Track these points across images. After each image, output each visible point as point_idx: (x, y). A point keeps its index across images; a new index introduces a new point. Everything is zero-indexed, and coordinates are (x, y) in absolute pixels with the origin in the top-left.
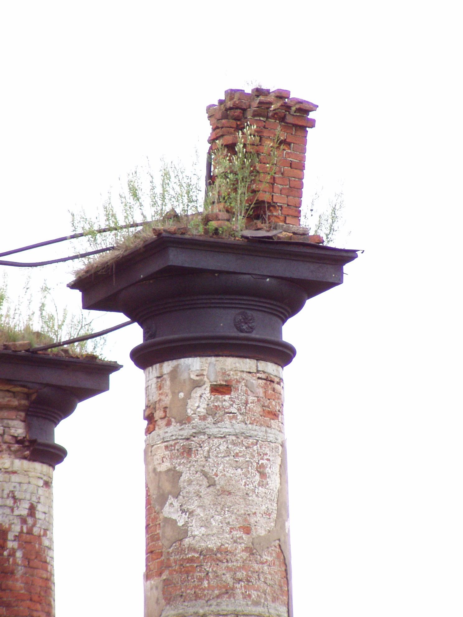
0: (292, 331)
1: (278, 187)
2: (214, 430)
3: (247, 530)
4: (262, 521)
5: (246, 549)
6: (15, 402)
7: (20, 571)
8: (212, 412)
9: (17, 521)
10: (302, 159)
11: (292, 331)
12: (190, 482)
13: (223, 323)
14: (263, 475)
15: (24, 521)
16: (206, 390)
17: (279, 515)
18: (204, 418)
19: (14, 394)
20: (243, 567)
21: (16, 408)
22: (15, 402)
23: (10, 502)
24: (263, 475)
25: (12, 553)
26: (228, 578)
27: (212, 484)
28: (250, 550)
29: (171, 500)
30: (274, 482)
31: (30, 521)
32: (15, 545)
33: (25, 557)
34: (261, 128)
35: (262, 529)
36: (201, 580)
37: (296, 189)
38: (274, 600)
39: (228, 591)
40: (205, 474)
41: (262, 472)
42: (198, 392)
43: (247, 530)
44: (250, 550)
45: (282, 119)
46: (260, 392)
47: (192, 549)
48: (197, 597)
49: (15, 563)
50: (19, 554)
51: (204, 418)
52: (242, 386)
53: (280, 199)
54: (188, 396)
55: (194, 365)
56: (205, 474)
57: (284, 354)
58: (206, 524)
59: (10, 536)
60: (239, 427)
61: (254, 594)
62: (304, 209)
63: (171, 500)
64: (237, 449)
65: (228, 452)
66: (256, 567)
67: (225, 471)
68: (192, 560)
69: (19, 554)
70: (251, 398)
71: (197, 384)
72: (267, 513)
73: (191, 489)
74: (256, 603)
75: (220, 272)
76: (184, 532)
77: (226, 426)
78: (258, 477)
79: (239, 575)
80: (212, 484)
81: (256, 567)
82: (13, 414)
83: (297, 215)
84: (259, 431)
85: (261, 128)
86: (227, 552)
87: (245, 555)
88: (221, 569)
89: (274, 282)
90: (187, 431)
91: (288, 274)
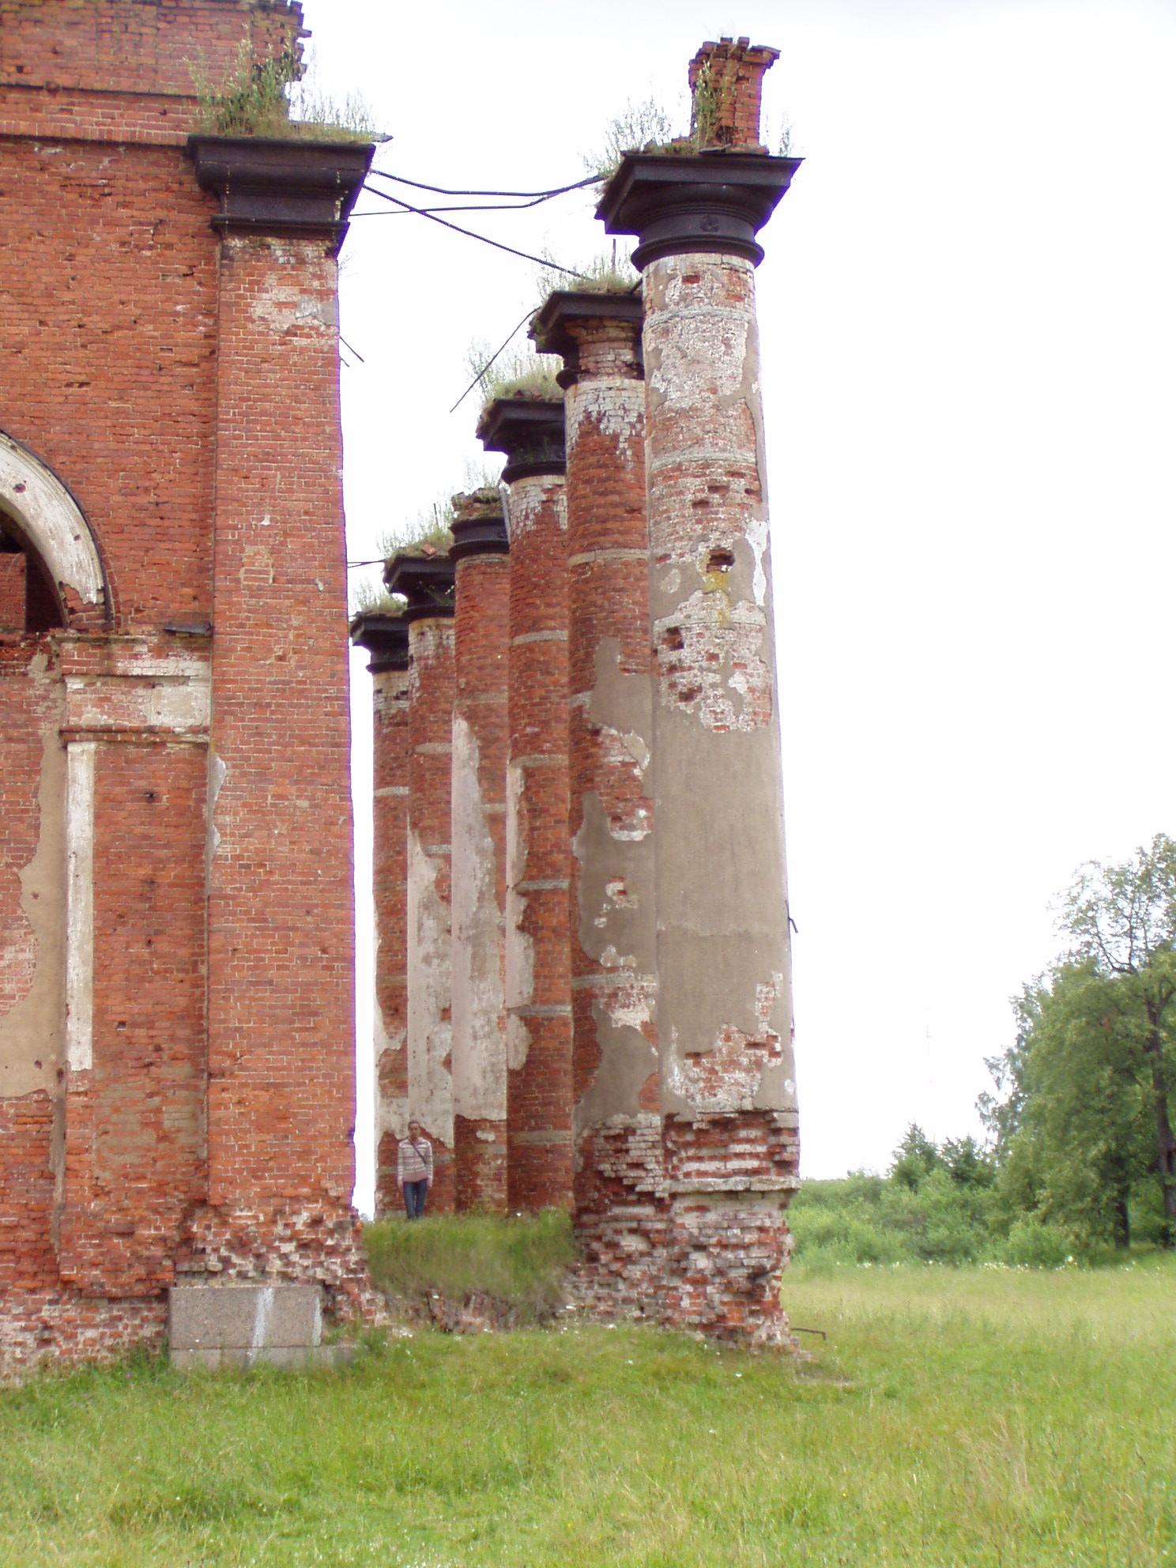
0: (761, 238)
1: (738, 114)
2: (685, 313)
3: (714, 391)
4: (728, 383)
5: (713, 406)
6: (623, 335)
7: (630, 465)
8: (684, 298)
9: (628, 427)
10: (760, 91)
11: (761, 238)
12: (668, 356)
13: (692, 226)
14: (728, 346)
15: (633, 426)
16: (679, 281)
17: (745, 377)
18: (677, 304)
19: (623, 329)
20: (711, 421)
21: (625, 340)
22: (623, 335)
23: (621, 413)
24: (728, 346)
25: (624, 452)
26: (698, 431)
27: (684, 356)
28: (717, 407)
29: (656, 372)
30: (740, 351)
31: (638, 426)
32: (626, 445)
33: (634, 454)
34: (731, 69)
35: (728, 389)
36: (677, 434)
37: (754, 116)
38: (740, 447)
39: (699, 442)
40: (679, 349)
41: (726, 343)
42: (673, 283)
43: (714, 391)
44: (717, 407)
45: (740, 59)
46: (725, 280)
47: (670, 410)
48: (675, 448)
49: (626, 460)
50: (629, 453)
51: (677, 304)
52: (708, 276)
53: (739, 124)
54: (666, 288)
55: (669, 262)
56: (679, 349)
57: (756, 255)
58: (680, 388)
59: (622, 439)
60: (706, 308)
61: (721, 443)
62: (762, 130)
63: (656, 372)
64: (705, 326)
65: (697, 330)
66: (723, 420)
67: (694, 344)
68: (670, 419)
69: (629, 453)
70: (716, 285)
71: (672, 277)
72: (733, 377)
73: (669, 362)
74: (724, 450)
75: (683, 183)
76: (664, 397)
77: (695, 309)
78: (723, 348)
79: (707, 428)
80: (684, 356)
81: (723, 420)
82: (622, 344)
83: (757, 136)
84: (725, 311)
85: (731, 69)
86: (697, 409)
87: (712, 411)
88: (693, 424)
89: (731, 189)
90: (666, 315)
91: (741, 181)
